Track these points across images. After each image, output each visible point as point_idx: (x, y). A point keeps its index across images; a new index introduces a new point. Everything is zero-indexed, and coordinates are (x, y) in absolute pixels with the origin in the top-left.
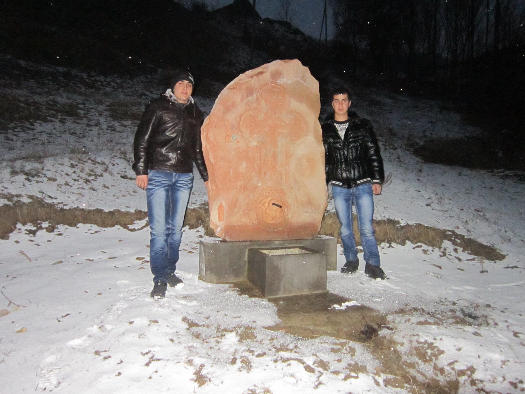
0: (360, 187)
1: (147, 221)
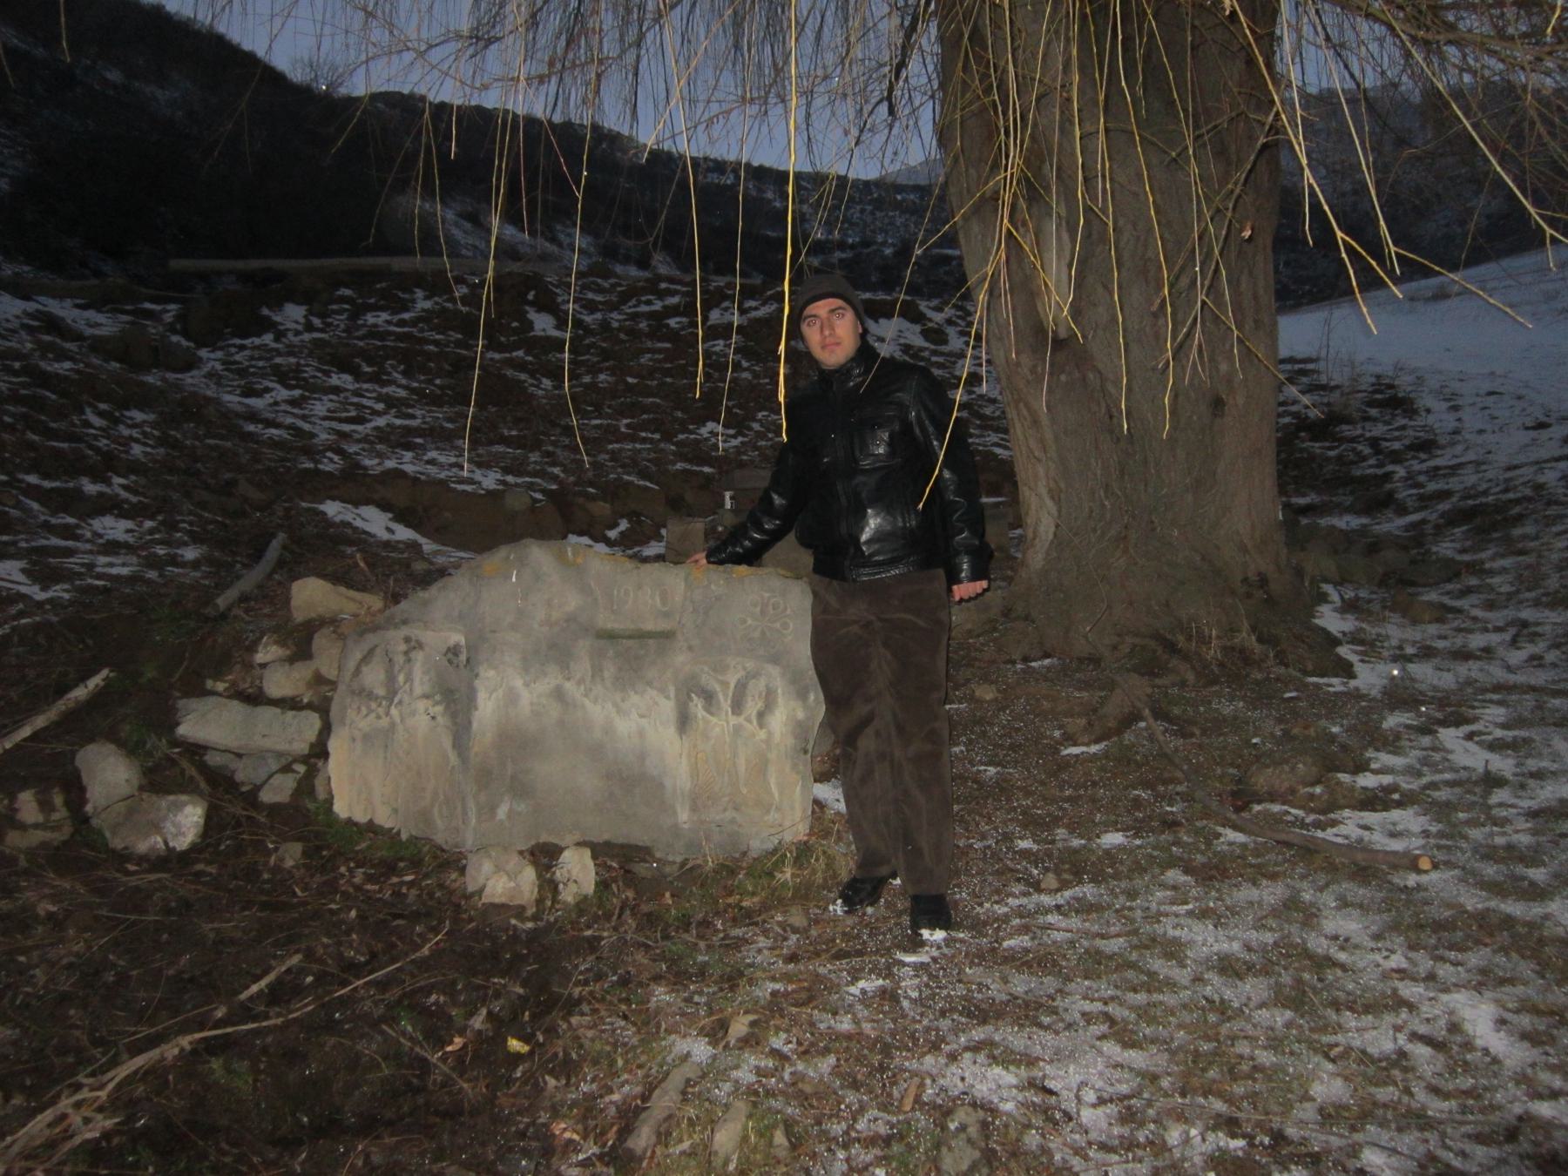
1: (182, 1050)
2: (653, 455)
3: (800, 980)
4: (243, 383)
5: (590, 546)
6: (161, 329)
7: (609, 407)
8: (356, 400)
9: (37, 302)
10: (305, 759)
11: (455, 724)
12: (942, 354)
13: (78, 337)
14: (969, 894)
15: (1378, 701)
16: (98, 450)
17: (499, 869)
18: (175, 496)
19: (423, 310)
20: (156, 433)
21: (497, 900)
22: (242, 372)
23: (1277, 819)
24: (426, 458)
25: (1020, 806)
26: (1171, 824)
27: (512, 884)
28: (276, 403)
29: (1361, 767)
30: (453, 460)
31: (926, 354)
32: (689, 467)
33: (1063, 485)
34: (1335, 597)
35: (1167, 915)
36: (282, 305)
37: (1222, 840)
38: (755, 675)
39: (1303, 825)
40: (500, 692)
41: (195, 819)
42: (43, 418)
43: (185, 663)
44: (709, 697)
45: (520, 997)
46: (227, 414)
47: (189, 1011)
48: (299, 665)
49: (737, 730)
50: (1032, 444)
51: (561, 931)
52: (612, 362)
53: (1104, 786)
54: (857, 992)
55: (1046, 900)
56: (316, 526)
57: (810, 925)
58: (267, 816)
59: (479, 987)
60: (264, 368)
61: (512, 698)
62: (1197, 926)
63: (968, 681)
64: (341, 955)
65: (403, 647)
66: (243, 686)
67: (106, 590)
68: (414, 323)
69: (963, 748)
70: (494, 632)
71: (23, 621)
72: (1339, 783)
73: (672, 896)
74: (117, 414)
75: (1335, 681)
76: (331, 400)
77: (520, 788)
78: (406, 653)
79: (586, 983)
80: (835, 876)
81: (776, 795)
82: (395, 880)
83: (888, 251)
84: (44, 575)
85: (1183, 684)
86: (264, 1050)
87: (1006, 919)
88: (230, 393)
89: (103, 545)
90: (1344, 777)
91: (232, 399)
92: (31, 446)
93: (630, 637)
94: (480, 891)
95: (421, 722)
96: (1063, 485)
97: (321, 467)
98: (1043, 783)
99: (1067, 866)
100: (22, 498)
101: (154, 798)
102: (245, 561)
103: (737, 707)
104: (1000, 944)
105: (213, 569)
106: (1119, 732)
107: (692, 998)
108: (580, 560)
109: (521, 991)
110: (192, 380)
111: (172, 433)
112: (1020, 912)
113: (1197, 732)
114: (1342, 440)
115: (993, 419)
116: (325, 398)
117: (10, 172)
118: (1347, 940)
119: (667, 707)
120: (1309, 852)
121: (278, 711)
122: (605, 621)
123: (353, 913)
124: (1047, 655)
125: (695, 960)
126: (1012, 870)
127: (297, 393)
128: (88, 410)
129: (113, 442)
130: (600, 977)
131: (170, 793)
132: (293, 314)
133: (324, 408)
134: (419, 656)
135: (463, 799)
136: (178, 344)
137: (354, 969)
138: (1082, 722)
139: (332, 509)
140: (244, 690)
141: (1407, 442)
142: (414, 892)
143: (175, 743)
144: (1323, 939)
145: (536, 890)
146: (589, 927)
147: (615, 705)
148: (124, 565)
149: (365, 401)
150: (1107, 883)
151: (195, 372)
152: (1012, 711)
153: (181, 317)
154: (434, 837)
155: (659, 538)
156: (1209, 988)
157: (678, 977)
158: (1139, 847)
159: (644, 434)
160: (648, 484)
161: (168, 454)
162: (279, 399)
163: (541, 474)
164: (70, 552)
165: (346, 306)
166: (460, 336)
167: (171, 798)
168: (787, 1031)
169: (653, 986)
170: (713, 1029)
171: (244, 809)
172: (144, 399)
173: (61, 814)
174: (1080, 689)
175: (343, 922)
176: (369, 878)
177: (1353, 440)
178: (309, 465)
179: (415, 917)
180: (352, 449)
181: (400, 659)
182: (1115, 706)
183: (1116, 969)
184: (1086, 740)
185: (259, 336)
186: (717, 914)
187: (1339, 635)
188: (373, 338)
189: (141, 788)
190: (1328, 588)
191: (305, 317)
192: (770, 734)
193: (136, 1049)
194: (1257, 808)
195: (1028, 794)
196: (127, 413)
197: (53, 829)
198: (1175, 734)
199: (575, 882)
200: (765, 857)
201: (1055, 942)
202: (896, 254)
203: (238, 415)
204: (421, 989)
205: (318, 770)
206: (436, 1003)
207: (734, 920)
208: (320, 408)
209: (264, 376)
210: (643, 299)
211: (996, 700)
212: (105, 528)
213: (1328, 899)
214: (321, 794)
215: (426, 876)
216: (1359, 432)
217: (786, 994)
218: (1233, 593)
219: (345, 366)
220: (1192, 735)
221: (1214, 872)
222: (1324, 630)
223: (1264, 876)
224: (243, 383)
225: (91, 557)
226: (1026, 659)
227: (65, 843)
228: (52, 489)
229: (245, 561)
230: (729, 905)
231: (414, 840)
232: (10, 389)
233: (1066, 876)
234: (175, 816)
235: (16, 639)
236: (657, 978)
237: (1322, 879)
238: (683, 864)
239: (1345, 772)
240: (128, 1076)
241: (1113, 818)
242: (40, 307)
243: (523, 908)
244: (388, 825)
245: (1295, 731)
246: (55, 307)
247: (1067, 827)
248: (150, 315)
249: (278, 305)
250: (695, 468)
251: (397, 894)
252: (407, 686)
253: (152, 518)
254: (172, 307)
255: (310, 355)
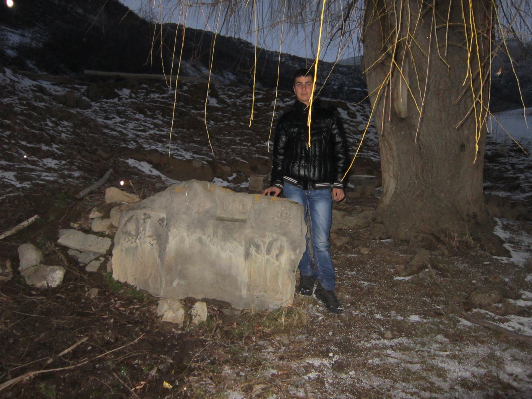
0: (318, 191)
1: (30, 377)
2: (247, 151)
3: (284, 370)
4: (105, 115)
5: (222, 182)
6: (79, 94)
7: (233, 133)
8: (144, 124)
9: (38, 82)
10: (104, 256)
11: (160, 248)
12: (354, 122)
13: (50, 95)
14: (355, 336)
15: (523, 268)
16: (49, 134)
17: (170, 308)
18: (75, 153)
19: (171, 94)
20: (71, 130)
21: (168, 321)
22: (105, 111)
23: (483, 316)
24: (166, 146)
25: (377, 300)
26: (439, 314)
27: (174, 315)
28: (116, 123)
29: (518, 297)
30: (176, 147)
31: (348, 122)
32: (260, 156)
33: (399, 173)
34: (499, 223)
35: (438, 356)
36: (122, 89)
37: (460, 323)
38: (276, 240)
39: (494, 320)
40: (178, 237)
41: (60, 276)
42: (31, 122)
43: (65, 215)
44: (258, 247)
45: (171, 364)
46: (97, 125)
47: (40, 358)
48: (105, 220)
49: (268, 261)
50: (388, 156)
51: (191, 336)
52: (235, 117)
53: (411, 294)
54: (307, 378)
55: (386, 342)
56: (124, 168)
57: (290, 344)
58: (87, 276)
59: (155, 359)
60: (113, 110)
61: (182, 240)
62: (451, 363)
63: (358, 245)
64: (104, 338)
65: (143, 217)
66: (84, 226)
67: (43, 185)
68: (167, 98)
69: (355, 273)
70: (177, 214)
71: (10, 194)
72: (509, 303)
73: (237, 324)
74: (58, 122)
75: (504, 258)
76: (135, 123)
77: (183, 275)
78: (144, 219)
79: (197, 362)
80: (301, 323)
81: (281, 288)
82: (132, 307)
83: (335, 87)
84: (21, 178)
85: (443, 255)
86: (64, 379)
87: (370, 349)
88: (100, 118)
89: (46, 169)
90: (511, 301)
91: (100, 120)
92: (25, 131)
93: (229, 221)
94: (163, 316)
95: (148, 246)
96: (399, 173)
97: (128, 146)
98: (386, 291)
99: (395, 328)
100: (19, 149)
101: (45, 266)
102: (96, 178)
103: (268, 251)
104: (367, 361)
105: (84, 180)
106: (417, 272)
107: (239, 372)
108: (212, 189)
109: (172, 361)
110: (88, 112)
111: (77, 130)
112: (375, 347)
113: (449, 275)
114: (501, 163)
115: (371, 146)
116: (133, 122)
117: (43, 41)
118: (517, 376)
119: (241, 250)
120: (498, 333)
121: (95, 236)
122: (219, 213)
123: (112, 321)
124: (388, 238)
125: (242, 354)
126: (373, 327)
127: (123, 120)
128: (48, 120)
129: (55, 132)
130: (203, 360)
131: (51, 265)
132: (126, 92)
133: (132, 126)
134: (149, 221)
135: (161, 277)
136: (85, 100)
137: (108, 345)
138: (403, 267)
139: (131, 162)
140: (84, 227)
141: (525, 166)
142: (138, 313)
143: (57, 245)
144: (506, 375)
145: (184, 318)
146: (203, 335)
147: (221, 246)
148: (52, 176)
149: (147, 125)
150: (412, 338)
151: (89, 110)
152: (375, 259)
153: (87, 90)
154: (149, 291)
155: (247, 181)
156: (457, 393)
157: (235, 362)
158: (426, 323)
159: (245, 143)
160: (245, 161)
161: (74, 138)
162: (117, 121)
163: (207, 155)
164: (33, 170)
165: (144, 91)
166: (183, 104)
167: (51, 267)
168: (277, 394)
169: (224, 366)
170: (247, 388)
171: (80, 273)
172: (69, 117)
173: (9, 270)
174: (401, 253)
175: (107, 324)
176: (122, 305)
177: (505, 163)
178: (125, 146)
179: (136, 323)
180: (140, 141)
181: (142, 221)
182: (416, 261)
183: (416, 379)
184: (404, 274)
185: (113, 99)
186: (254, 334)
187: (504, 239)
188: (153, 103)
189: (41, 262)
190: (497, 219)
191: (130, 93)
192: (280, 263)
193: (15, 375)
194: (474, 310)
195: (380, 295)
196: (62, 122)
197: (5, 275)
198: (440, 275)
199: (199, 316)
200: (275, 312)
201: (390, 363)
202: (338, 88)
203: (101, 126)
204: (132, 357)
205: (109, 260)
206: (137, 364)
207: (260, 337)
208: (131, 125)
209: (113, 113)
210: (249, 95)
211: (368, 254)
212: (48, 163)
213: (507, 355)
214: (109, 270)
215: (144, 306)
216: (507, 161)
217: (278, 376)
218: (463, 220)
219: (141, 112)
220: (447, 276)
221: (458, 338)
222: (498, 237)
223: (479, 341)
224: (105, 115)
225: (41, 173)
226: (381, 238)
227: (9, 281)
228: (31, 147)
229: (96, 178)
230: (259, 330)
231: (141, 291)
232: (20, 111)
233: (395, 333)
234: (52, 274)
235: (7, 201)
236: (226, 362)
237: (504, 346)
238: (242, 311)
239: (511, 298)
240: (6, 388)
241: (415, 309)
242: (39, 84)
243: (177, 325)
244: (132, 284)
245: (490, 279)
246: (45, 84)
247: (395, 310)
248: (77, 89)
249: (121, 89)
250: (262, 157)
251: (131, 313)
252: (143, 232)
253: (65, 160)
254: (85, 87)
255: (130, 107)
